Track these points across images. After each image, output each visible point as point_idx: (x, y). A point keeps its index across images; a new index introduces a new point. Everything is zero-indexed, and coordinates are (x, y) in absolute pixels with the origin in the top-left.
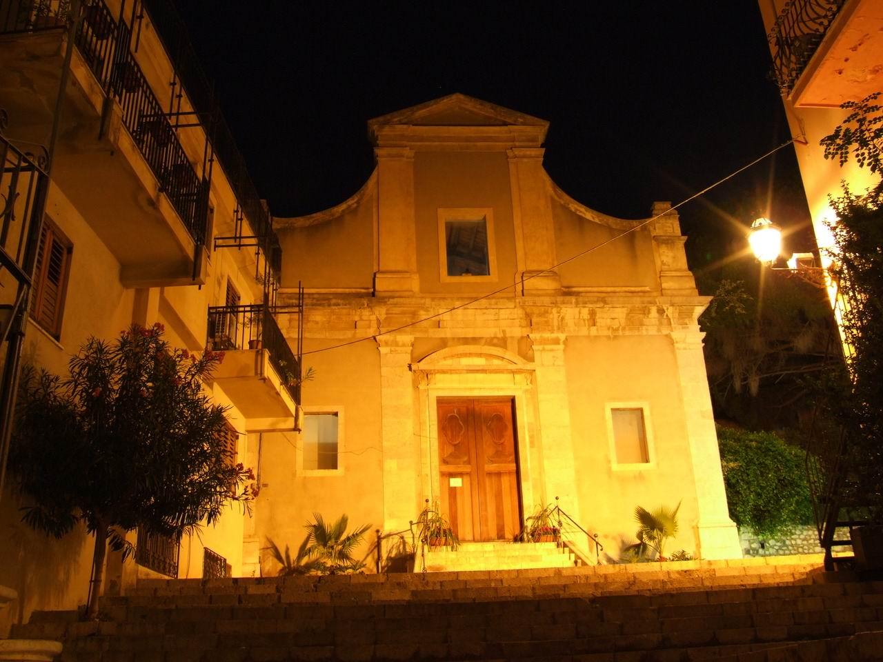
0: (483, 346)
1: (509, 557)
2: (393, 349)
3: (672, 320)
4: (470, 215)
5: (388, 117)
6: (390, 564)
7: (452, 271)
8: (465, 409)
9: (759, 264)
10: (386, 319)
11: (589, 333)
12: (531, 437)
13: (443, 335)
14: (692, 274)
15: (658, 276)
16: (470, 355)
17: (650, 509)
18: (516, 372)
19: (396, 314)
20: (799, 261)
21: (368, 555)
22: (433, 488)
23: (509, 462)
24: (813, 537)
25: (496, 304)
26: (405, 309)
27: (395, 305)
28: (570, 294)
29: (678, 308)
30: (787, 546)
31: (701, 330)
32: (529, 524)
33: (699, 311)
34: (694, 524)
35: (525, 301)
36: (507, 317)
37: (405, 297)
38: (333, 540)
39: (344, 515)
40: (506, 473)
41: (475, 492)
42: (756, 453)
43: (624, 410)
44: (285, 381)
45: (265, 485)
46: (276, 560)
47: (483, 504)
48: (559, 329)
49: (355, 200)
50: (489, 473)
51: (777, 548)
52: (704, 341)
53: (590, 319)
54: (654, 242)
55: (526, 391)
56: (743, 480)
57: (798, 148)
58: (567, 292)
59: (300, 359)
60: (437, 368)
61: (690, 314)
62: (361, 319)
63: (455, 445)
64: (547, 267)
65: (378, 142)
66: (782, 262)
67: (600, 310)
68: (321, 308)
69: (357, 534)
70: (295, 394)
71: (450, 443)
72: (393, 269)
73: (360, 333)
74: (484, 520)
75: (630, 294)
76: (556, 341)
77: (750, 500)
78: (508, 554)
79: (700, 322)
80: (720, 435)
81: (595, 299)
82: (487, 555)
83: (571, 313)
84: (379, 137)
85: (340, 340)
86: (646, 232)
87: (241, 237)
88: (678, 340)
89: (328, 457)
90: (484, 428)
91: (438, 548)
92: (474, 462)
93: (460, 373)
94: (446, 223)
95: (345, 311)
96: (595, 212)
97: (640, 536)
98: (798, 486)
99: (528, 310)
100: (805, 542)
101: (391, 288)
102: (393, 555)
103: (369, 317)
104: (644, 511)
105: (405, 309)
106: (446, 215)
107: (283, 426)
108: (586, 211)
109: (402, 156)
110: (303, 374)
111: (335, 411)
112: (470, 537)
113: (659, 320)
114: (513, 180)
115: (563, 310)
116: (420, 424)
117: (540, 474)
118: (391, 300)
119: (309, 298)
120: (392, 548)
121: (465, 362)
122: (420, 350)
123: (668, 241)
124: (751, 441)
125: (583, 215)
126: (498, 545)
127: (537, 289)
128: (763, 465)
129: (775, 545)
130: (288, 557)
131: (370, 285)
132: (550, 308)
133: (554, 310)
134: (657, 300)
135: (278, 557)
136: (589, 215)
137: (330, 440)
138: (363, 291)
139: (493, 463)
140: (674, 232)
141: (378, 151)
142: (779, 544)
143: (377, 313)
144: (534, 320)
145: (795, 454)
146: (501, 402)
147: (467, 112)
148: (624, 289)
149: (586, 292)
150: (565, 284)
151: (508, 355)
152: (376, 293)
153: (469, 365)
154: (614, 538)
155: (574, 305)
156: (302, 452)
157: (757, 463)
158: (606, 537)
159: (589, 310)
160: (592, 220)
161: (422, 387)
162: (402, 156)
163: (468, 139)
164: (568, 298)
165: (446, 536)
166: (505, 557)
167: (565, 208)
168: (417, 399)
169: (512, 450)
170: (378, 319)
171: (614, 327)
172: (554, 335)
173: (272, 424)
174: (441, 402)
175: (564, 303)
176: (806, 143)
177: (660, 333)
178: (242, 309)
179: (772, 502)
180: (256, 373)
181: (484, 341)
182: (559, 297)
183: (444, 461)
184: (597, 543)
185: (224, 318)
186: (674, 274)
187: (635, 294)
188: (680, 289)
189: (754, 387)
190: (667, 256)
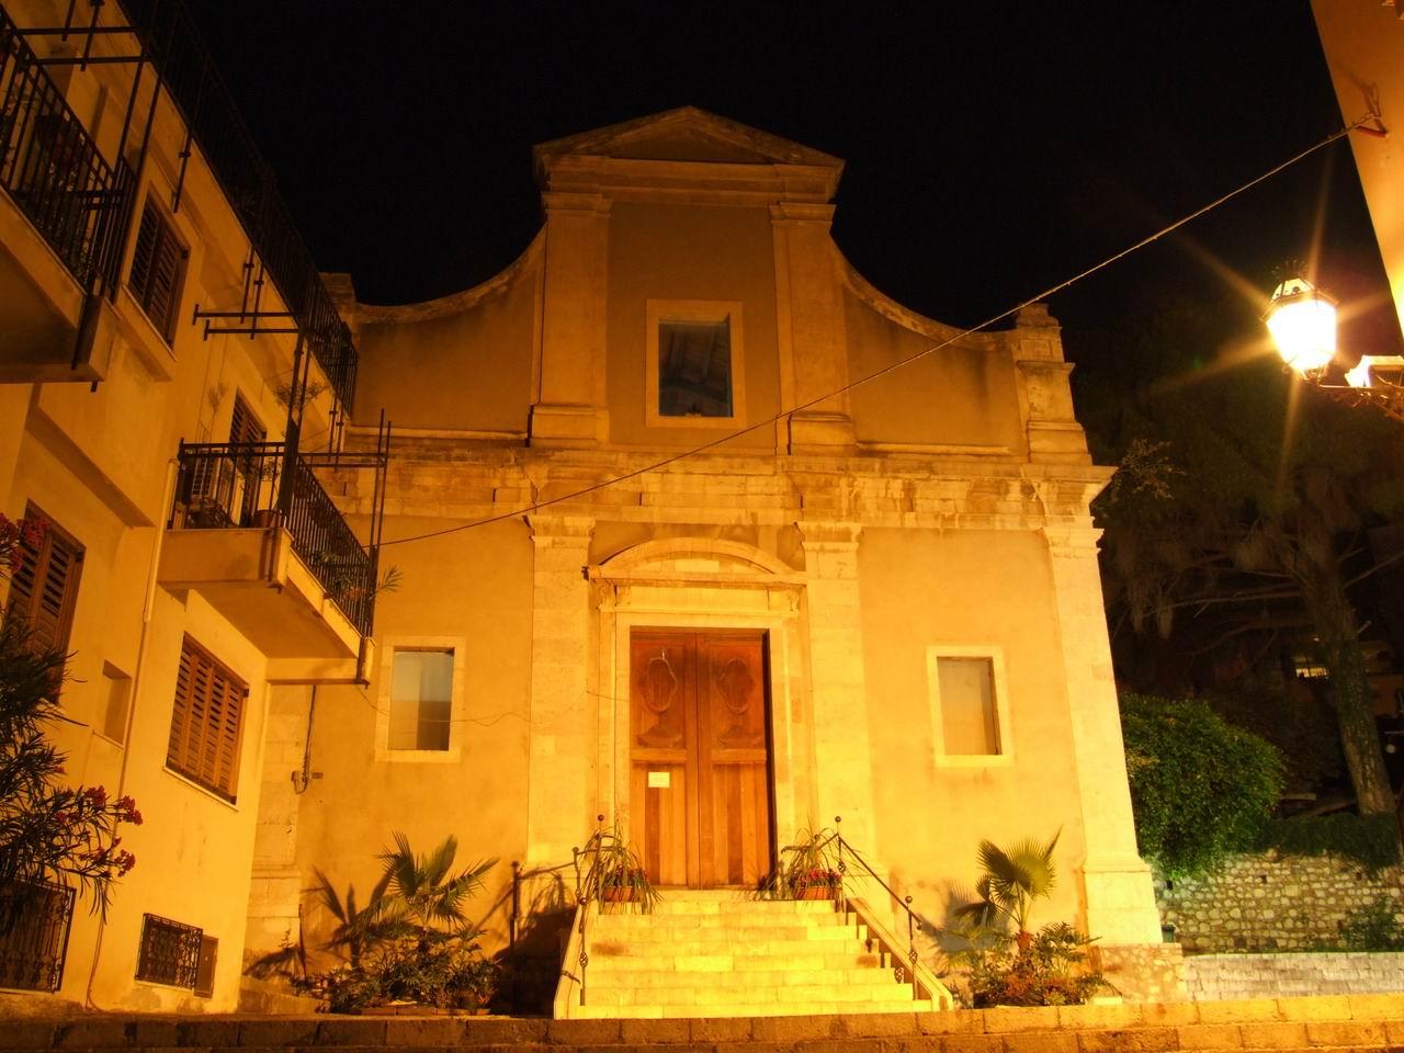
0: (716, 539)
1: (745, 930)
2: (557, 539)
3: (1045, 505)
4: (702, 313)
5: (569, 140)
6: (534, 926)
7: (669, 406)
8: (680, 649)
9: (1288, 376)
10: (547, 487)
11: (902, 524)
12: (796, 703)
13: (646, 519)
14: (1081, 428)
15: (1024, 429)
16: (693, 554)
17: (1004, 846)
18: (771, 587)
19: (565, 478)
20: (1374, 372)
21: (495, 908)
22: (618, 789)
23: (755, 747)
24: (1252, 872)
25: (742, 467)
26: (581, 470)
27: (565, 462)
28: (871, 454)
29: (1056, 485)
30: (1209, 886)
31: (1096, 525)
32: (787, 859)
33: (1093, 490)
34: (1076, 866)
35: (793, 464)
36: (759, 491)
37: (583, 450)
38: (427, 885)
39: (451, 837)
40: (748, 765)
41: (693, 799)
42: (1177, 738)
43: (959, 660)
44: (333, 591)
45: (318, 775)
46: (329, 912)
47: (706, 821)
48: (850, 514)
49: (506, 279)
50: (720, 766)
52: (1100, 543)
53: (904, 499)
54: (1017, 372)
55: (789, 622)
56: (1152, 783)
57: (1362, 146)
58: (867, 451)
59: (375, 552)
60: (633, 575)
61: (1076, 497)
62: (504, 486)
63: (661, 714)
64: (831, 405)
65: (549, 183)
66: (1336, 373)
67: (923, 483)
68: (433, 463)
69: (469, 876)
70: (362, 617)
71: (653, 710)
72: (565, 399)
73: (501, 508)
74: (706, 850)
75: (976, 459)
76: (845, 536)
77: (1163, 817)
78: (745, 922)
79: (1093, 512)
80: (1124, 709)
81: (915, 464)
82: (706, 924)
83: (870, 486)
84: (552, 175)
85: (464, 521)
87: (256, 314)
88: (1056, 541)
89: (434, 729)
90: (713, 684)
91: (618, 905)
92: (692, 744)
93: (675, 586)
94: (660, 326)
95: (475, 471)
96: (918, 316)
97: (983, 888)
98: (1244, 795)
99: (798, 480)
100: (1239, 881)
101: (560, 433)
102: (541, 908)
103: (519, 482)
104: (995, 849)
105: (581, 470)
106: (665, 312)
107: (335, 674)
108: (904, 314)
109: (590, 208)
110: (380, 579)
111: (450, 645)
112: (679, 879)
113: (1023, 506)
114: (779, 256)
115: (860, 482)
116: (599, 673)
118: (557, 453)
119: (414, 445)
120: (540, 895)
121: (684, 566)
122: (606, 543)
123: (1042, 371)
124: (1168, 716)
125: (897, 320)
126: (726, 895)
128: (1188, 760)
129: (1191, 885)
130: (351, 905)
131: (524, 427)
132: (836, 478)
133: (843, 482)
134: (1021, 470)
135: (334, 905)
136: (907, 320)
137: (439, 698)
138: (510, 436)
139: (726, 748)
141: (551, 200)
143: (531, 474)
144: (808, 497)
145: (1241, 740)
146: (744, 639)
147: (706, 141)
148: (964, 449)
149: (899, 452)
150: (864, 435)
151: (759, 557)
152: (532, 441)
153: (691, 573)
154: (936, 888)
155: (877, 474)
156: (388, 718)
157: (1178, 754)
158: (921, 885)
159: (904, 483)
160: (913, 329)
161: (606, 608)
162: (590, 208)
163: (704, 185)
164: (867, 461)
165: (633, 884)
166: (739, 929)
167: (865, 306)
168: (596, 631)
169: (762, 725)
170: (533, 487)
171: (947, 515)
172: (841, 525)
173: (318, 670)
174: (639, 636)
175: (860, 470)
176: (1383, 132)
177: (1025, 528)
179: (1198, 820)
180: (262, 576)
181: (717, 531)
182: (852, 459)
183: (640, 741)
185: (211, 466)
186: (1052, 426)
187: (983, 459)
188: (1061, 453)
189: (1165, 623)
190: (1040, 395)
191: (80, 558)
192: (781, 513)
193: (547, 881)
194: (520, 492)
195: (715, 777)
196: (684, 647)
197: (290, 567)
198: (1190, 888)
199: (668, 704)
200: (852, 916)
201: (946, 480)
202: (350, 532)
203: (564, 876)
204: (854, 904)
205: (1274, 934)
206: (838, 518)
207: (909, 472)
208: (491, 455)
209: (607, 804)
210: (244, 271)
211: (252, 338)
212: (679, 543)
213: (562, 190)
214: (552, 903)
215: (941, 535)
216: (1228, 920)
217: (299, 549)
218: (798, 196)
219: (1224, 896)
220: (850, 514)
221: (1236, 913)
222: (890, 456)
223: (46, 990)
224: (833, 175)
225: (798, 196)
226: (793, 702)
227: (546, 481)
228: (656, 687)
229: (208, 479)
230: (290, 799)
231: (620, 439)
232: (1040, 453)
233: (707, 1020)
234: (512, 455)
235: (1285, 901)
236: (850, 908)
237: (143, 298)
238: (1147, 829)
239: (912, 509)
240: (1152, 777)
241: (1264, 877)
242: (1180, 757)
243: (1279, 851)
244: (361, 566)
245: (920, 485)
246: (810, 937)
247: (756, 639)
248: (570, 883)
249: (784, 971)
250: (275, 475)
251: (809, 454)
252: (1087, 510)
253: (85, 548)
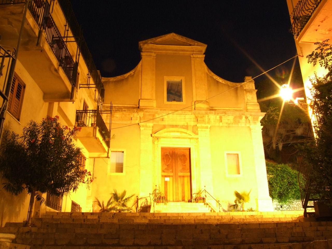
4: (176, 79)
5: (147, 41)
6: (141, 209)
7: (169, 99)
10: (143, 117)
14: (258, 104)
16: (174, 131)
17: (240, 192)
18: (191, 139)
19: (147, 115)
21: (133, 205)
23: (187, 172)
27: (147, 112)
28: (213, 110)
29: (253, 116)
30: (291, 207)
32: (194, 196)
33: (261, 118)
38: (120, 199)
41: (174, 183)
45: (96, 178)
47: (177, 188)
48: (208, 123)
49: (133, 72)
54: (245, 92)
56: (275, 182)
58: (211, 109)
59: (110, 131)
61: (257, 119)
63: (167, 165)
70: (108, 144)
71: (166, 165)
73: (133, 122)
74: (177, 194)
75: (235, 111)
76: (207, 128)
77: (277, 190)
79: (261, 122)
83: (213, 117)
84: (143, 48)
86: (242, 88)
87: (89, 84)
89: (120, 168)
91: (160, 203)
96: (223, 80)
97: (236, 202)
98: (296, 185)
99: (197, 116)
100: (297, 206)
101: (145, 105)
102: (143, 205)
103: (137, 116)
106: (168, 79)
109: (151, 56)
111: (123, 151)
112: (172, 200)
114: (193, 66)
119: (114, 108)
122: (156, 129)
123: (250, 91)
124: (279, 167)
125: (219, 81)
126: (183, 203)
129: (286, 207)
132: (205, 115)
133: (207, 116)
135: (100, 205)
136: (221, 80)
137: (120, 162)
141: (142, 54)
142: (288, 206)
144: (199, 119)
146: (185, 150)
150: (211, 106)
151: (189, 132)
152: (140, 107)
159: (219, 116)
160: (222, 82)
161: (156, 143)
162: (151, 56)
163: (176, 50)
164: (212, 111)
165: (163, 199)
167: (212, 77)
170: (140, 117)
171: (229, 123)
177: (246, 126)
178: (89, 111)
180: (93, 136)
183: (163, 171)
187: (237, 111)
189: (280, 147)
192: (193, 123)
193: (144, 200)
194: (137, 118)
195: (179, 179)
196: (172, 151)
197: (98, 135)
198: (286, 207)
199: (169, 163)
200: (208, 206)
201: (229, 115)
203: (147, 199)
204: (208, 203)
206: (205, 124)
207: (221, 114)
208: (131, 110)
212: (172, 129)
213: (145, 52)
214: (145, 204)
218: (197, 53)
220: (208, 123)
222: (217, 110)
224: (205, 48)
225: (197, 53)
227: (143, 116)
228: (166, 160)
229: (82, 117)
231: (159, 107)
232: (249, 110)
233: (181, 213)
234: (135, 110)
236: (207, 204)
238: (274, 192)
239: (221, 122)
240: (275, 181)
242: (281, 176)
245: (223, 117)
247: (188, 149)
248: (149, 200)
251: (199, 110)
252: (260, 122)
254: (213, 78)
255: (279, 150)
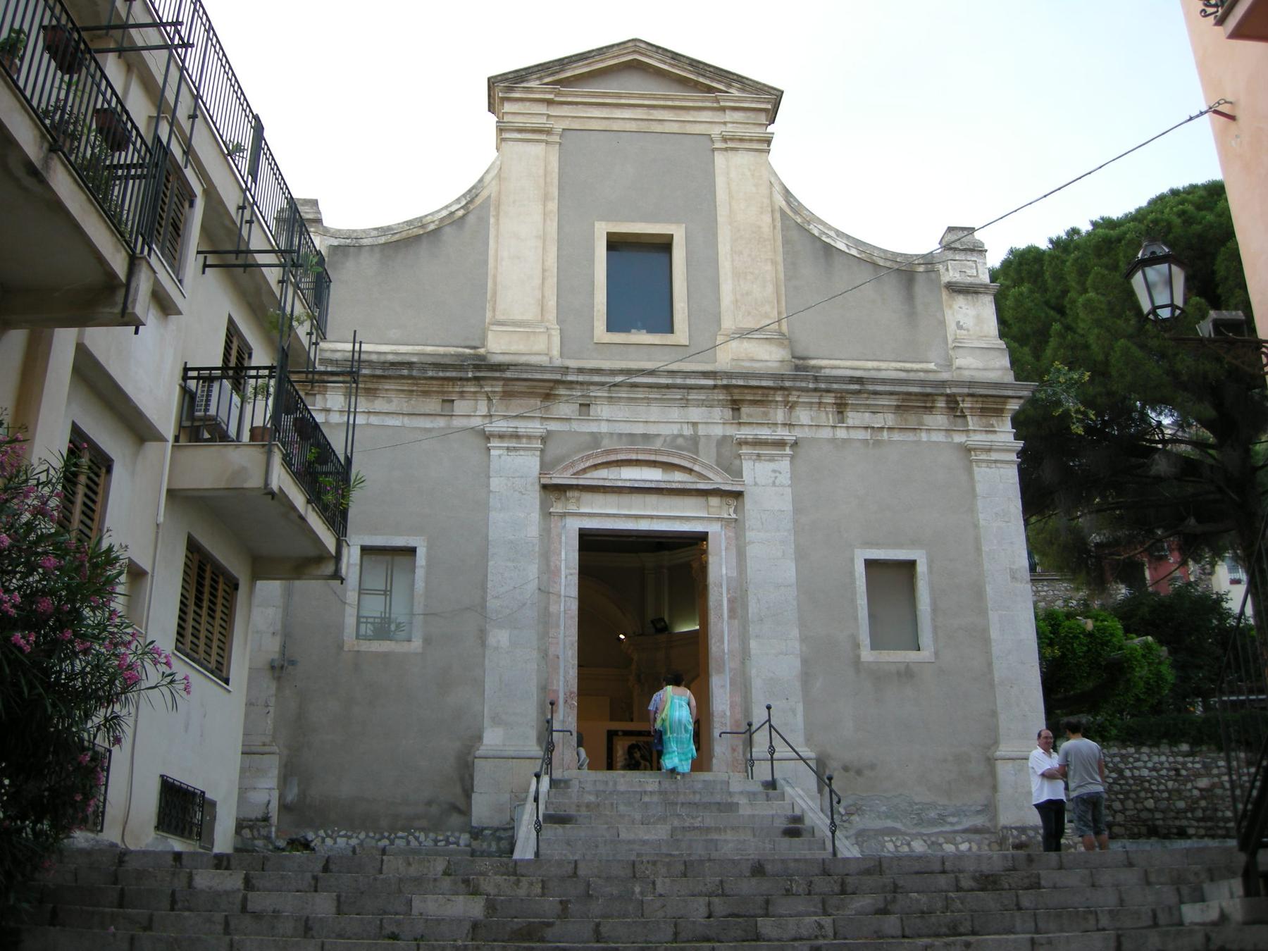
1: (683, 804)
20: (1217, 324)
24: (1167, 765)
51: (1111, 781)
59: (349, 460)
86: (933, 275)
100: (1154, 774)
101: (514, 348)
117: (743, 663)
127: (753, 360)
138: (468, 351)
140: (977, 276)
142: (1114, 775)
160: (847, 251)
178: (253, 373)
184: (831, 791)
191: (109, 470)
202: (329, 444)
205: (1184, 823)
209: (557, 692)
210: (238, 213)
211: (245, 272)
215: (871, 446)
216: (1142, 810)
217: (287, 461)
219: (1139, 788)
221: (1150, 803)
223: (92, 831)
226: (729, 600)
230: (268, 687)
235: (1196, 792)
237: (160, 245)
241: (1177, 770)
243: (1192, 745)
244: (338, 473)
246: (741, 812)
249: (717, 840)
250: (268, 395)
253: (112, 460)
254: (808, 231)
255: (1240, 631)
